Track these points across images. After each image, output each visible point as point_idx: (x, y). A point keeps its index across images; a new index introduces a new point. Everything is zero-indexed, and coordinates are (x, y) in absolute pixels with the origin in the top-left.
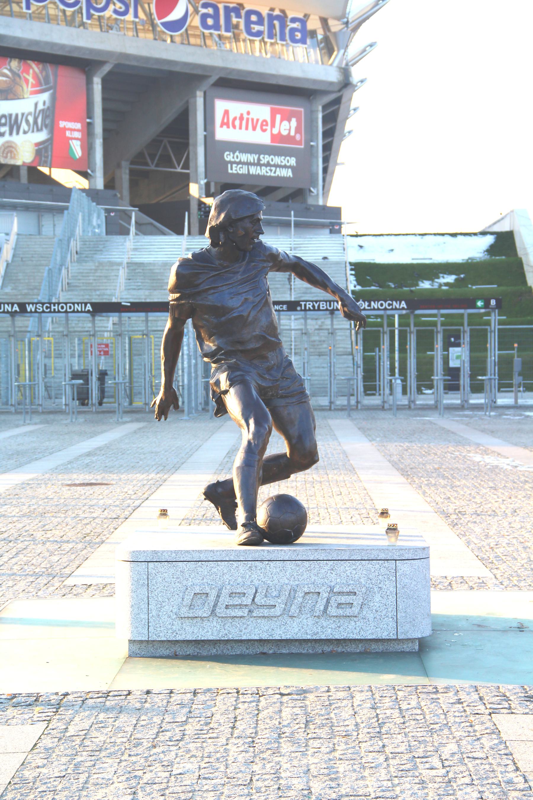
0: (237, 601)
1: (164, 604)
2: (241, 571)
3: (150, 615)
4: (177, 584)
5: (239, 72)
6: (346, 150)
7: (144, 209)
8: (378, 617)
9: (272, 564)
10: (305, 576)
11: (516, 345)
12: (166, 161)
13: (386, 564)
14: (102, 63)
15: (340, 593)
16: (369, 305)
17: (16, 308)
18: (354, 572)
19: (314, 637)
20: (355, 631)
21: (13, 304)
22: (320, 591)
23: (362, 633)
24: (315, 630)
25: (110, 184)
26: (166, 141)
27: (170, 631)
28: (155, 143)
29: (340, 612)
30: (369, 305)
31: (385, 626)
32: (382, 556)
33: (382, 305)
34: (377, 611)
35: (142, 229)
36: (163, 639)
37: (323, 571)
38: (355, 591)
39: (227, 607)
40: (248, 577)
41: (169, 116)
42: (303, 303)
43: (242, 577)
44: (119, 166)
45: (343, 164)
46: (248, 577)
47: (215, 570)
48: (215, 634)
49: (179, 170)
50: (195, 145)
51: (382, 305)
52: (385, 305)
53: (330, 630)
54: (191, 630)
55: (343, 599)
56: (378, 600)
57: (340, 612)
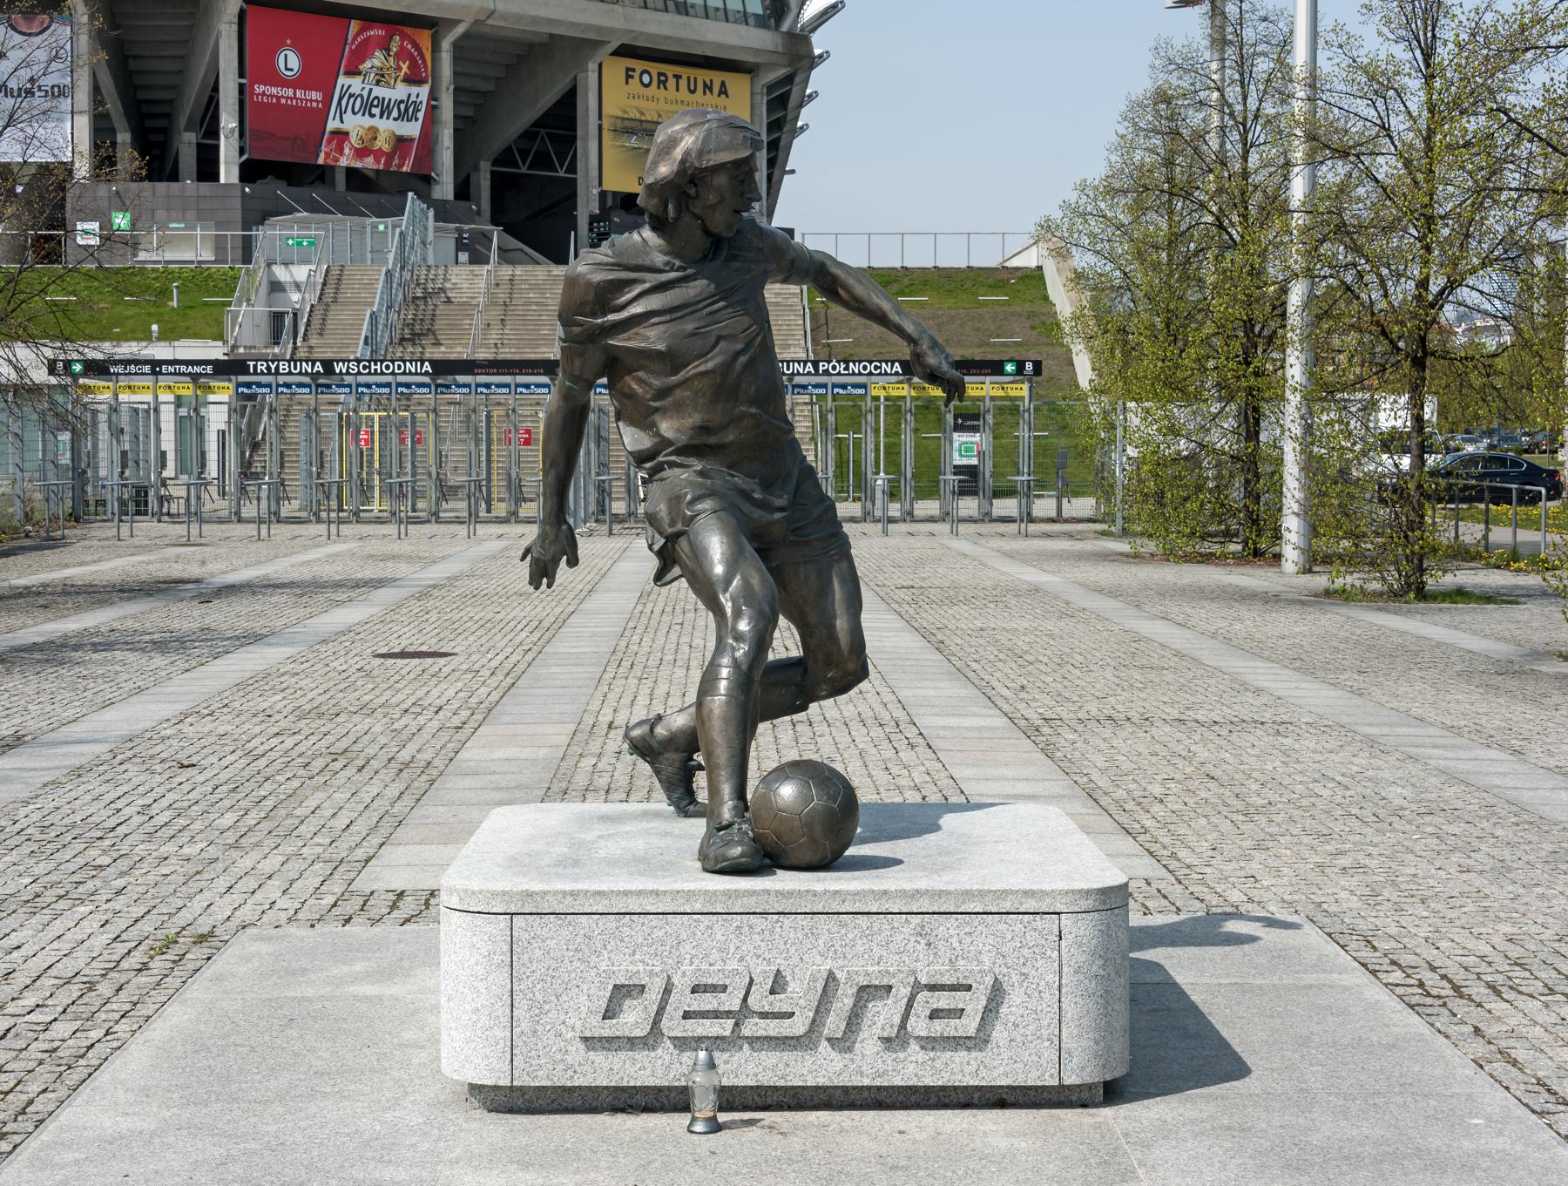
0: (708, 1002)
1: (547, 1007)
2: (719, 937)
3: (517, 1031)
4: (576, 964)
5: (650, 36)
6: (799, 153)
7: (510, 230)
8: (1019, 1039)
9: (787, 921)
10: (860, 949)
11: (155, 327)
12: (543, 161)
13: (1038, 922)
14: (455, 22)
15: (933, 988)
16: (847, 368)
17: (319, 367)
18: (969, 940)
19: (878, 1082)
20: (967, 1069)
21: (314, 363)
22: (892, 982)
23: (983, 1073)
24: (880, 1066)
25: (463, 190)
26: (543, 132)
27: (561, 1066)
28: (529, 135)
29: (938, 1027)
30: (847, 368)
31: (1034, 1057)
32: (1030, 905)
33: (865, 368)
34: (1016, 1025)
35: (506, 256)
36: (544, 1083)
37: (900, 937)
38: (969, 982)
39: (687, 1015)
40: (732, 950)
41: (549, 99)
42: (251, 364)
43: (721, 950)
44: (476, 168)
45: (793, 172)
46: (732, 950)
47: (661, 933)
48: (660, 1073)
49: (561, 174)
50: (586, 138)
51: (865, 368)
52: (870, 368)
53: (912, 1066)
54: (606, 1066)
55: (944, 1001)
56: (1018, 1001)
57: (938, 1027)
